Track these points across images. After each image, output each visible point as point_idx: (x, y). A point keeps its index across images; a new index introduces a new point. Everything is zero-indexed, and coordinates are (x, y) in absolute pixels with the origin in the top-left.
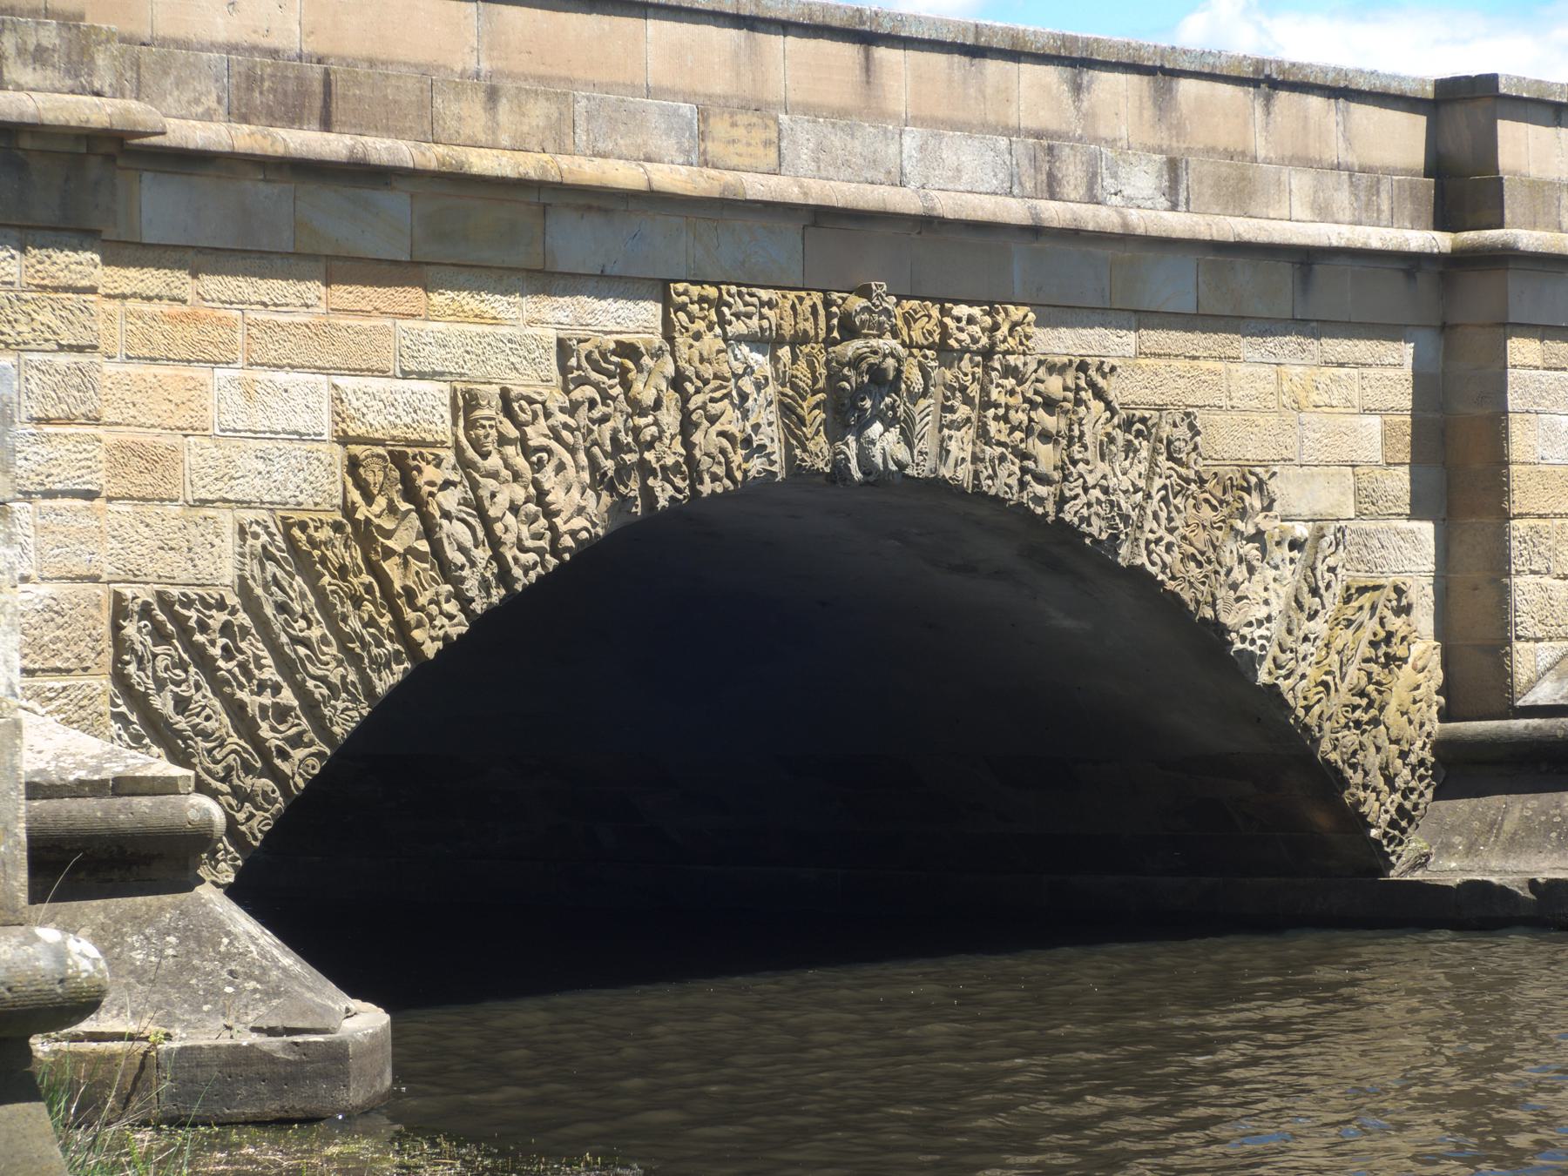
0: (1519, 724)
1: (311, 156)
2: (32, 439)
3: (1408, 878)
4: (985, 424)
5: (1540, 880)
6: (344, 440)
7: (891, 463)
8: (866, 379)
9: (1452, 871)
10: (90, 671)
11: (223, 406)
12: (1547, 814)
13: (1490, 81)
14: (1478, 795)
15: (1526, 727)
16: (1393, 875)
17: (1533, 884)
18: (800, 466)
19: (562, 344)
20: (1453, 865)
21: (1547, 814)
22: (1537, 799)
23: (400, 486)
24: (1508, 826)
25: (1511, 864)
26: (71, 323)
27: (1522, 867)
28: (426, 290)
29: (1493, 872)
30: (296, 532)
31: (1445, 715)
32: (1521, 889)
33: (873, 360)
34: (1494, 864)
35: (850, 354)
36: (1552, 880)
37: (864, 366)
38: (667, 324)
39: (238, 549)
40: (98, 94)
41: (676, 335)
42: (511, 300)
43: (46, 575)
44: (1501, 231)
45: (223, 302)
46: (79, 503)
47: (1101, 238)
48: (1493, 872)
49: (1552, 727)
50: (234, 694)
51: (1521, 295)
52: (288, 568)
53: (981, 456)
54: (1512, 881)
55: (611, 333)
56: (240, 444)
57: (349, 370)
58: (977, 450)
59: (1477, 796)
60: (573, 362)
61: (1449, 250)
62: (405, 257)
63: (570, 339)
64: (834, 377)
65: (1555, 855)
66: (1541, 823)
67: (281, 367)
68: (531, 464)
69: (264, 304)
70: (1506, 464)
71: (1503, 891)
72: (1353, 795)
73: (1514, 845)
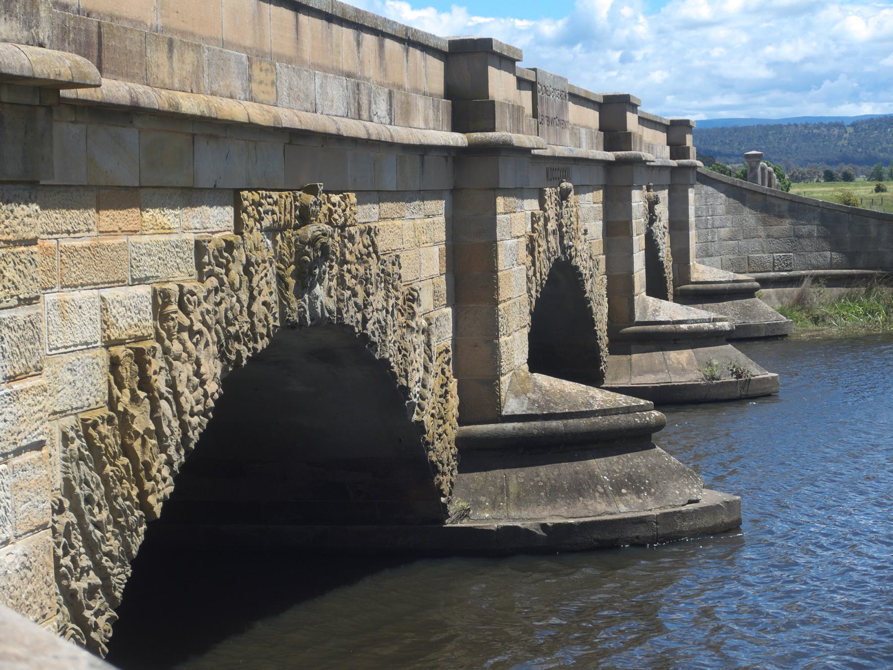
0: (509, 426)
1: (114, 101)
2: (7, 399)
3: (459, 525)
4: (343, 276)
5: (549, 524)
6: (109, 344)
7: (326, 312)
8: (319, 254)
9: (487, 519)
10: (47, 617)
11: (51, 327)
12: (533, 481)
13: (488, 42)
14: (486, 469)
15: (514, 428)
16: (448, 524)
17: (544, 526)
18: (288, 319)
19: (198, 244)
20: (487, 515)
21: (533, 481)
22: (523, 471)
23: (138, 378)
24: (513, 489)
25: (524, 514)
26: (25, 276)
27: (532, 515)
28: (142, 210)
29: (514, 520)
30: (91, 430)
31: (461, 422)
32: (537, 530)
33: (323, 240)
34: (513, 514)
35: (309, 236)
36: (557, 524)
37: (319, 245)
38: (238, 223)
39: (62, 455)
40: (41, 45)
41: (244, 231)
42: (177, 213)
43: (20, 532)
44: (490, 134)
45: (49, 233)
46: (34, 455)
47: (355, 141)
48: (514, 520)
49: (529, 428)
50: (69, 586)
51: (507, 174)
52: (90, 464)
53: (341, 298)
54: (531, 525)
55: (217, 232)
56: (59, 360)
57: (109, 283)
58: (338, 293)
59: (485, 470)
60: (206, 259)
61: (467, 145)
62: (137, 184)
63: (204, 241)
64: (300, 253)
65: (549, 507)
66: (531, 486)
67: (76, 286)
68: (194, 343)
69: (68, 232)
70: (496, 272)
71: (527, 531)
72: (438, 479)
73: (520, 501)
